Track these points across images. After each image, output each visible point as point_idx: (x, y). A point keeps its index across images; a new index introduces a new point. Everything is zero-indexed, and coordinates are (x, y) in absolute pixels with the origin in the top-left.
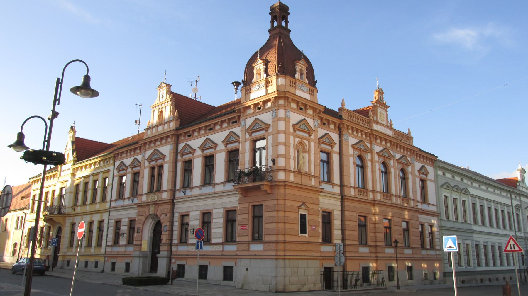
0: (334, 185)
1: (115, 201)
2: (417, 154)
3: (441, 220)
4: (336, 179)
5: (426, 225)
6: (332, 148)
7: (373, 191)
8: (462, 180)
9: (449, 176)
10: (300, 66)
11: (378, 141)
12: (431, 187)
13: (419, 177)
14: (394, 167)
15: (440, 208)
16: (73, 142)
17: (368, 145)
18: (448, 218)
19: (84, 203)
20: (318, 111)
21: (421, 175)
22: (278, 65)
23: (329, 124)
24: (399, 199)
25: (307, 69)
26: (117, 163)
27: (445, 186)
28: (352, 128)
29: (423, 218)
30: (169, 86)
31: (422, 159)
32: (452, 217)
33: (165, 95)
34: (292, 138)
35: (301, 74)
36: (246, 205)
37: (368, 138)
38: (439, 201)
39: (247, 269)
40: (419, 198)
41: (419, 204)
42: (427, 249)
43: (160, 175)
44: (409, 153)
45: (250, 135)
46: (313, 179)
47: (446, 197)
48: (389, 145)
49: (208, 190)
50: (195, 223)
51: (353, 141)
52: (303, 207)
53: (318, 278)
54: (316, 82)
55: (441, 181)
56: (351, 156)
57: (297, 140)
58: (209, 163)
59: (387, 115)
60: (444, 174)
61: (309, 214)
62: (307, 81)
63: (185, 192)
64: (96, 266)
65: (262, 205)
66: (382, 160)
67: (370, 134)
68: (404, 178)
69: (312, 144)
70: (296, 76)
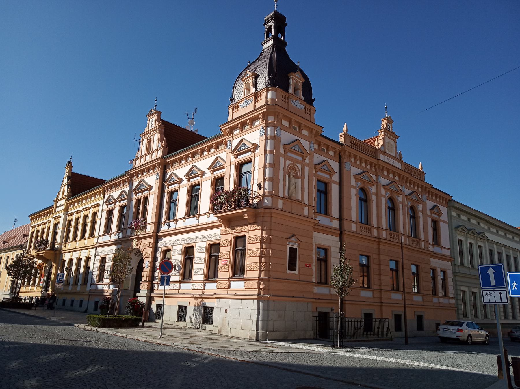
0: (332, 218)
1: (103, 236)
2: (429, 191)
3: (455, 265)
4: (335, 211)
5: (439, 270)
6: (331, 177)
7: (378, 228)
8: (478, 224)
9: (464, 218)
10: (295, 79)
11: (385, 173)
12: (444, 230)
13: (431, 217)
14: (402, 203)
15: (454, 253)
16: (68, 177)
17: (374, 177)
18: (463, 264)
19: (74, 239)
20: (314, 132)
21: (434, 215)
22: (269, 77)
23: (328, 149)
24: (407, 239)
25: (304, 84)
26: (106, 197)
27: (460, 229)
28: (355, 157)
29: (434, 262)
30: (159, 113)
31: (434, 198)
32: (467, 262)
33: (154, 123)
34: (282, 160)
35: (296, 90)
36: (229, 237)
37: (373, 169)
38: (453, 245)
39: (226, 311)
40: (431, 240)
41: (431, 246)
42: (440, 297)
43: (145, 208)
44: (420, 190)
45: (236, 158)
46: (306, 209)
47: (460, 241)
48: (397, 178)
49: (192, 222)
50: (176, 259)
51: (355, 170)
52: (293, 239)
53: (310, 324)
54: (314, 100)
55: (455, 223)
56: (353, 187)
57: (288, 162)
58: (194, 192)
59: (396, 146)
60: (459, 215)
61: (299, 248)
62: (302, 97)
63: (169, 225)
64: (81, 306)
65: (245, 236)
66: (388, 194)
67: (376, 165)
68: (414, 217)
69: (306, 168)
70: (290, 90)
